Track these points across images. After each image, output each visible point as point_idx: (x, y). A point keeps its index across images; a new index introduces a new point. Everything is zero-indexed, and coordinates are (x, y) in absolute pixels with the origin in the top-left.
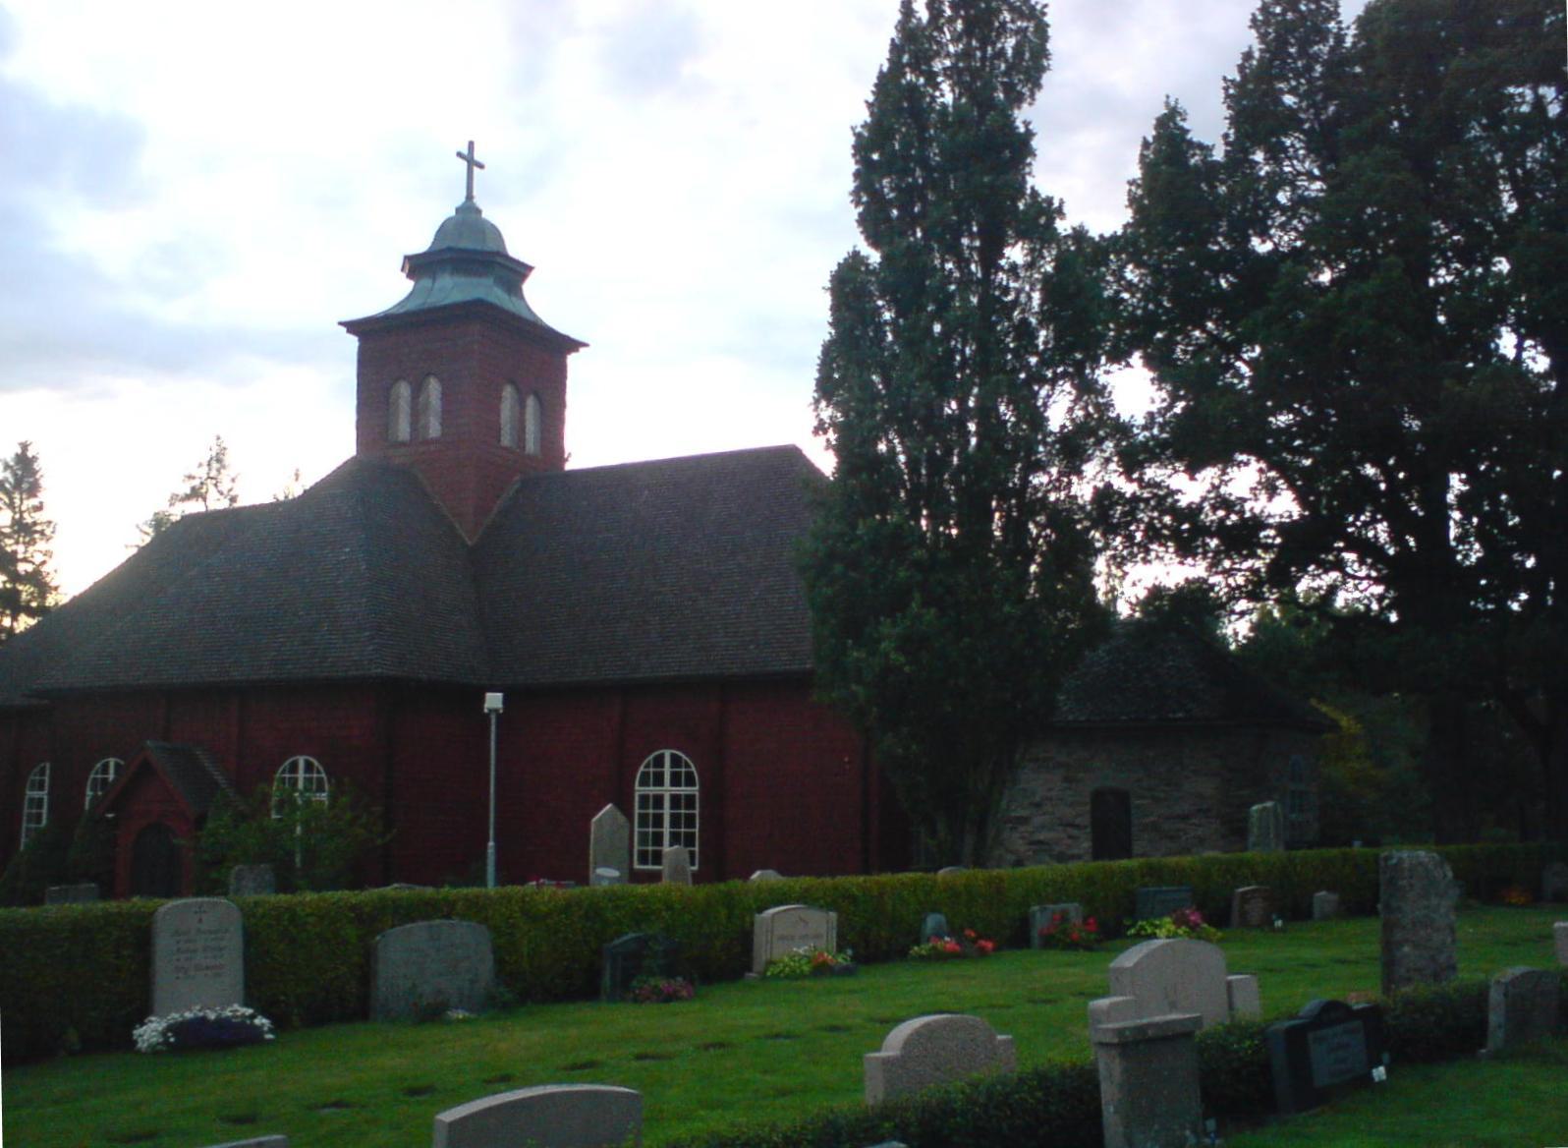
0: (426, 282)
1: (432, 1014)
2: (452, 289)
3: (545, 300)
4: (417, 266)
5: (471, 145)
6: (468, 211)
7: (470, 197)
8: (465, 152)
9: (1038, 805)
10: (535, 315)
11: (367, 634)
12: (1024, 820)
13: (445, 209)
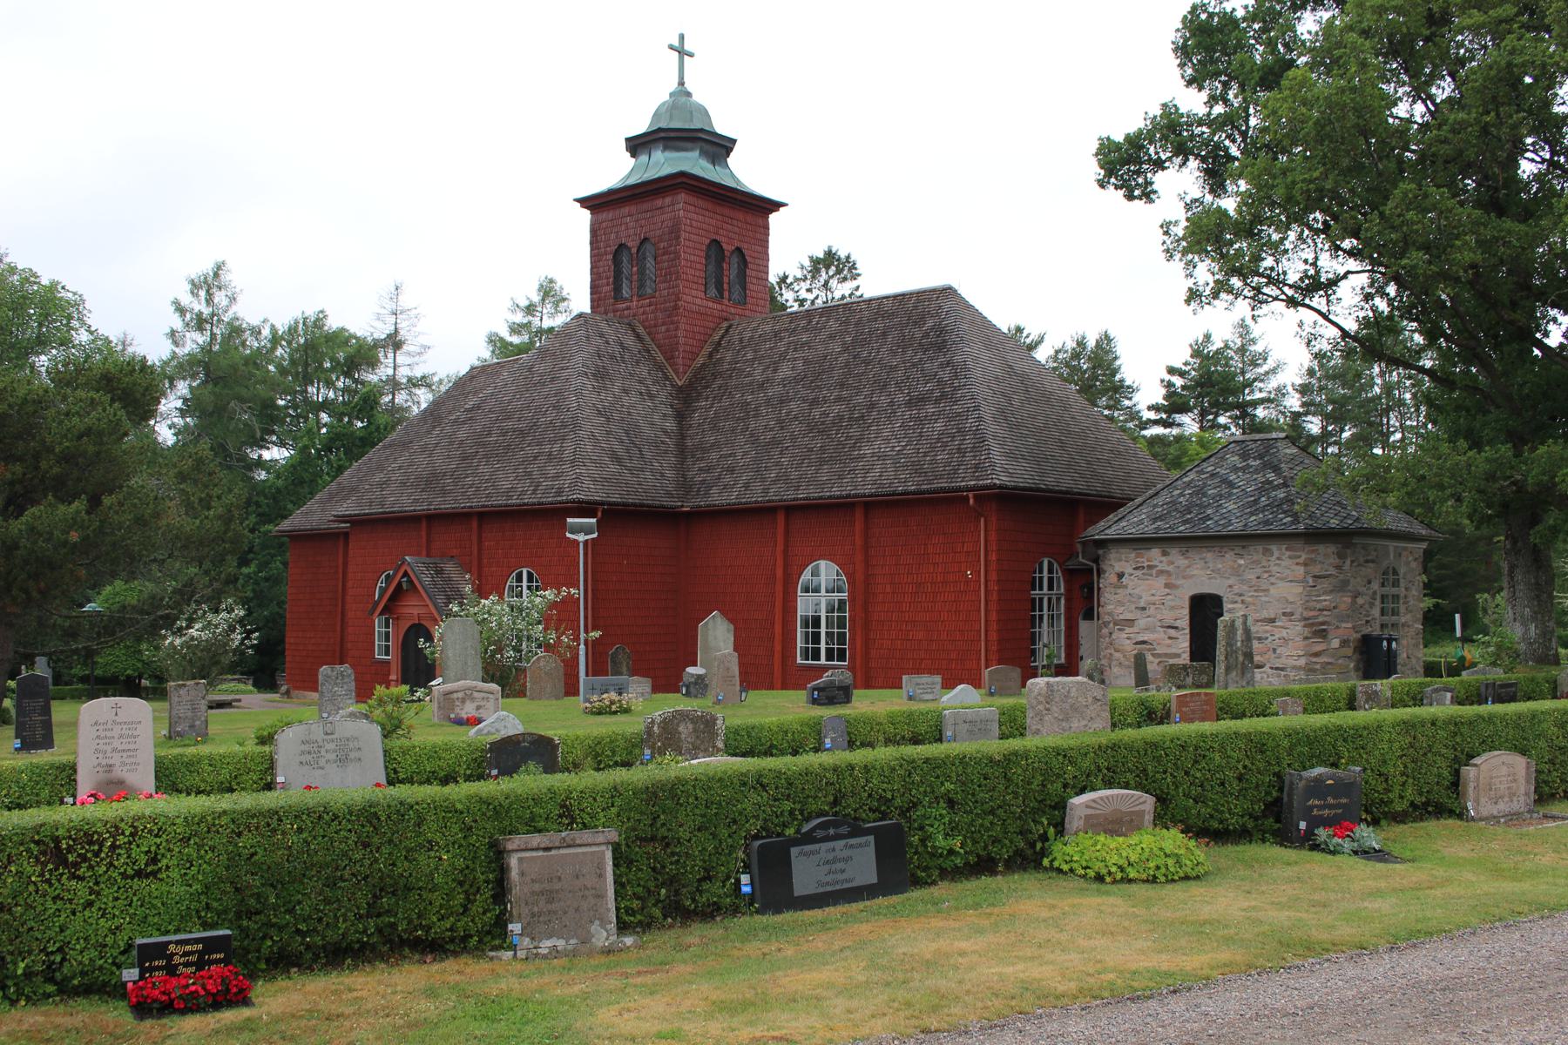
0: (644, 158)
1: (577, 766)
2: (663, 163)
3: (747, 170)
4: (636, 145)
5: (682, 37)
6: (682, 92)
7: (681, 83)
8: (676, 44)
9: (1144, 609)
10: (738, 181)
11: (81, 393)
12: (1131, 622)
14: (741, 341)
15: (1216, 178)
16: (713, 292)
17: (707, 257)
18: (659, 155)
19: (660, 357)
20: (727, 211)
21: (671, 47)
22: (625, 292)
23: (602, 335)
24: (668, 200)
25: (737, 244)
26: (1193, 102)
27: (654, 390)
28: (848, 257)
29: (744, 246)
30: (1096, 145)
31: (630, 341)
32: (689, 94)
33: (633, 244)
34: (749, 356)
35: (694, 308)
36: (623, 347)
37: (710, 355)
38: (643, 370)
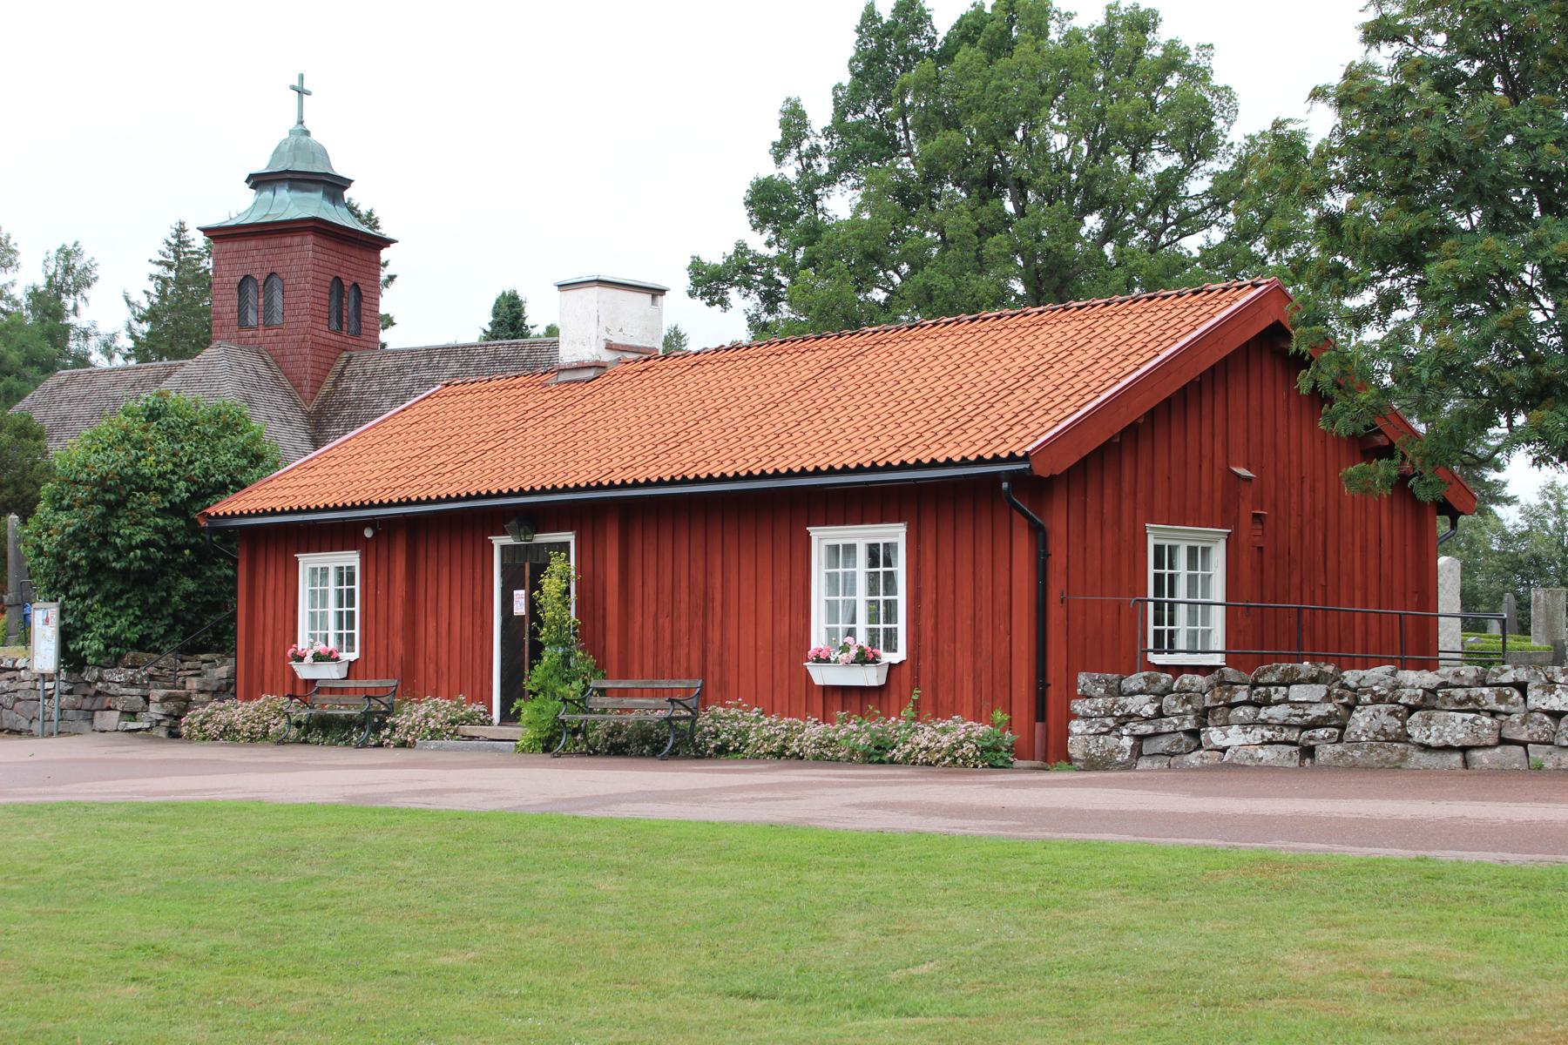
0: (268, 194)
2: (291, 205)
4: (258, 181)
5: (302, 77)
13: (278, 130)
14: (364, 372)
15: (771, 300)
16: (334, 326)
17: (331, 293)
18: (283, 194)
19: (288, 386)
20: (347, 250)
21: (293, 88)
22: (252, 319)
23: (240, 364)
24: (297, 240)
25: (354, 279)
26: (759, 243)
27: (289, 414)
28: (370, 214)
29: (360, 281)
30: (689, 263)
31: (262, 369)
32: (307, 133)
33: (260, 276)
34: (375, 388)
35: (321, 341)
36: (258, 375)
37: (335, 385)
38: (278, 398)
